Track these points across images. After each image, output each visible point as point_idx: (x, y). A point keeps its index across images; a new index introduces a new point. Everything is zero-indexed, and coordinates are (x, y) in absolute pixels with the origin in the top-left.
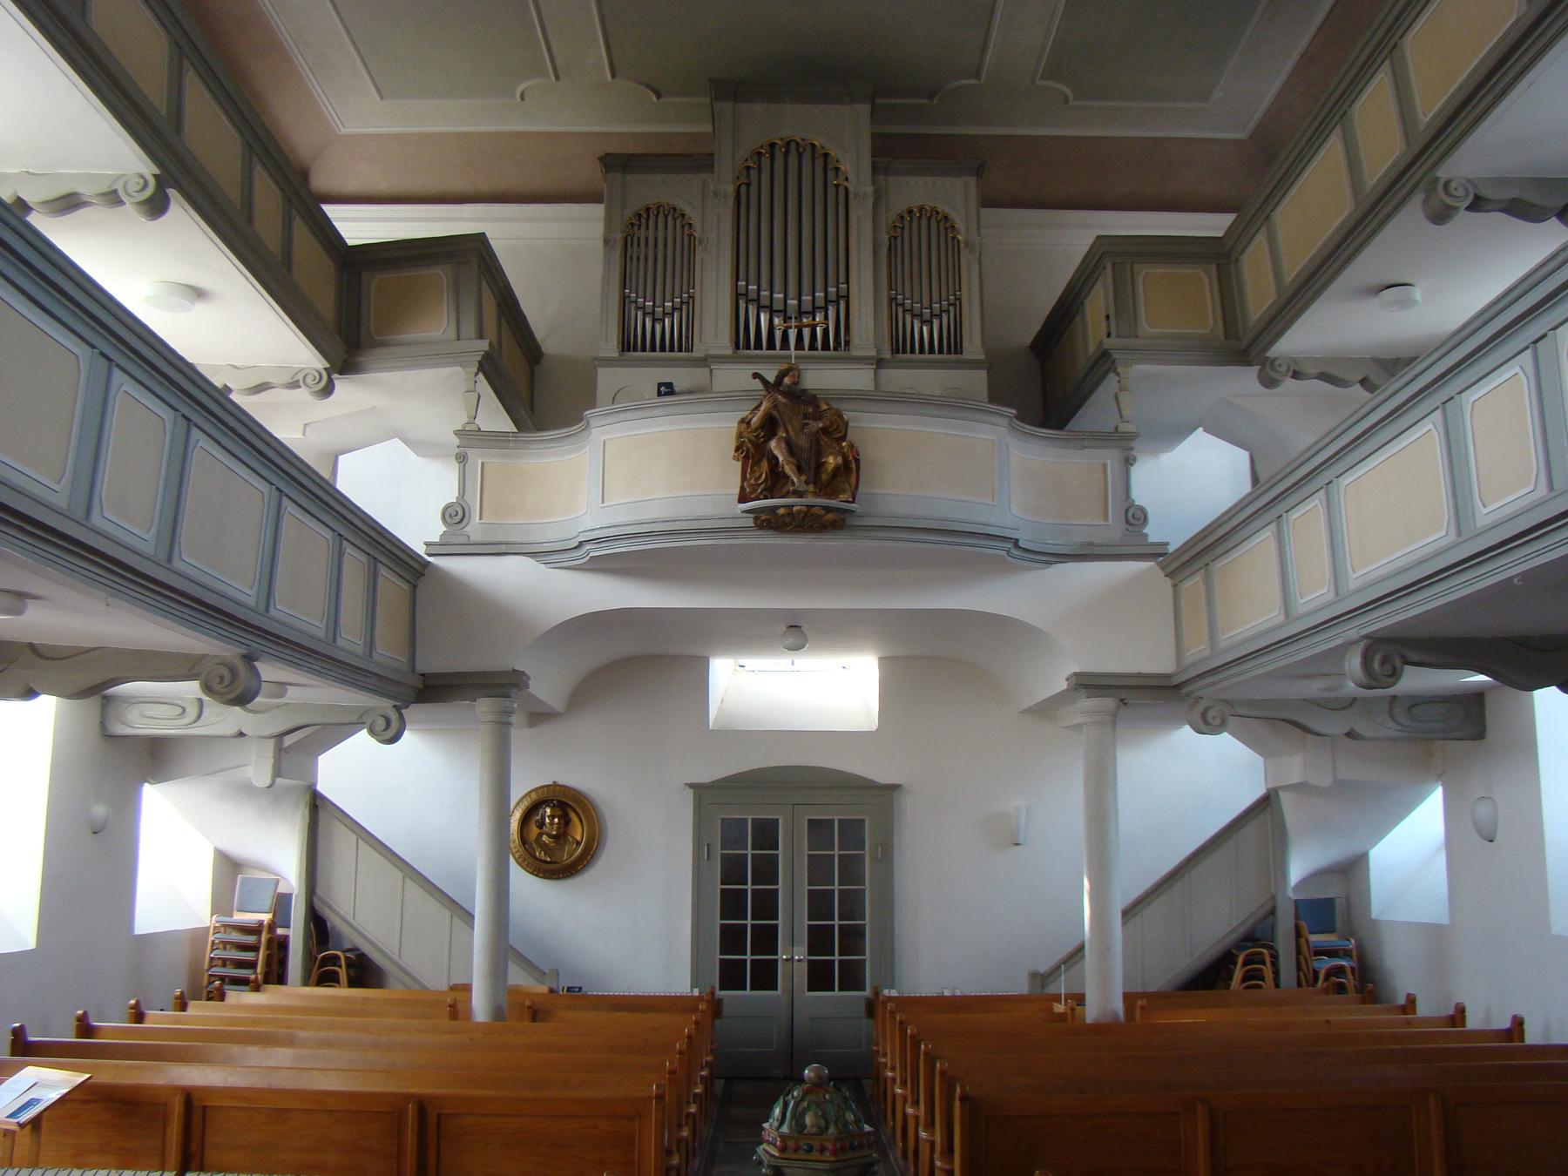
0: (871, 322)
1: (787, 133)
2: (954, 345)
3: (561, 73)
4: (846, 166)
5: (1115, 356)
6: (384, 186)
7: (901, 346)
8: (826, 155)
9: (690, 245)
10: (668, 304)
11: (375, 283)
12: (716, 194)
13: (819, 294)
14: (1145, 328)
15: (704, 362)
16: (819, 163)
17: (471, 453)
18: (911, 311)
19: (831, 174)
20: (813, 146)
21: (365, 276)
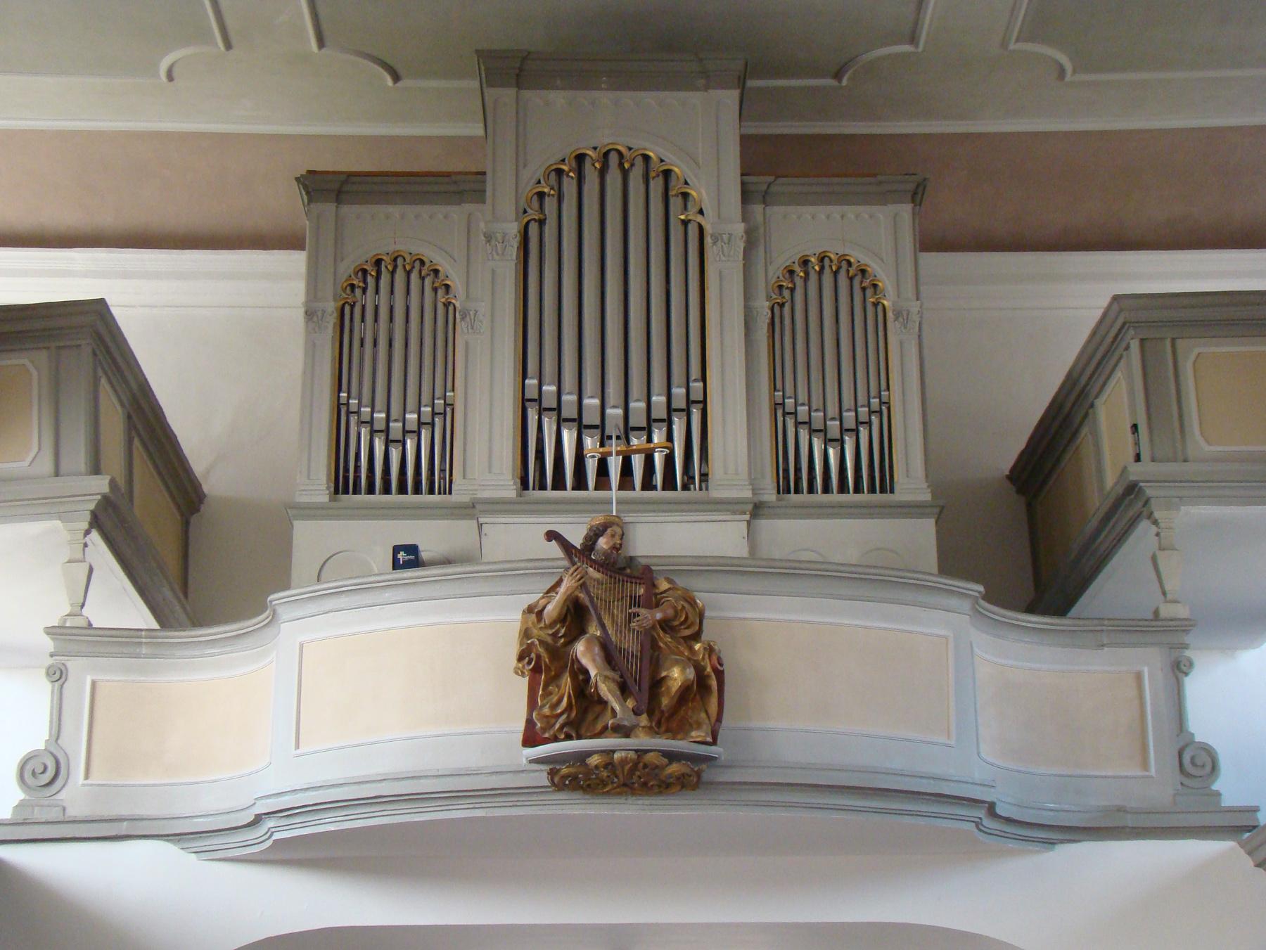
1: (605, 139)
4: (701, 192)
7: (792, 479)
8: (667, 174)
14: (1199, 444)
15: (470, 510)
16: (656, 186)
17: (74, 665)
19: (676, 203)
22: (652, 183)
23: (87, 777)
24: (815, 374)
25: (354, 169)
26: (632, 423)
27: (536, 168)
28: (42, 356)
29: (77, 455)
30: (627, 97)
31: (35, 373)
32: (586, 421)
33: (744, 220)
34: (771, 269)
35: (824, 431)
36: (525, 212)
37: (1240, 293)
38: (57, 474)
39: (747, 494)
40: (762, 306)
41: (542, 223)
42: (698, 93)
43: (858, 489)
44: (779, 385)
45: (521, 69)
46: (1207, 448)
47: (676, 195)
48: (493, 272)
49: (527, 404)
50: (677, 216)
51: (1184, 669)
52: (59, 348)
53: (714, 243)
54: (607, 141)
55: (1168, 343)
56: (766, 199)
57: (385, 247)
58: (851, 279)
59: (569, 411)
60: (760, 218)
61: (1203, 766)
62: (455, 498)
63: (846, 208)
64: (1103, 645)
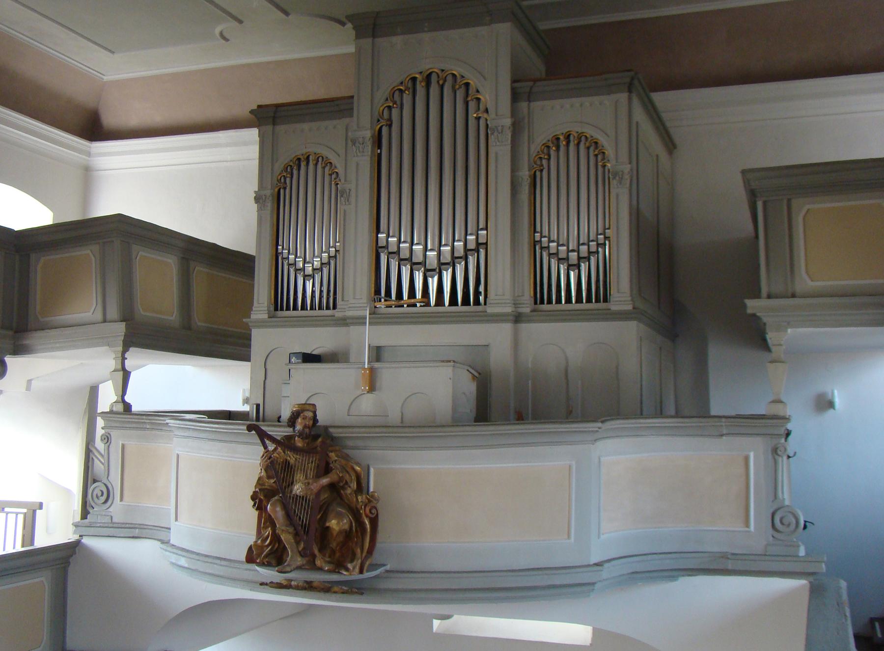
0: (508, 274)
1: (427, 65)
2: (599, 293)
3: (240, 17)
4: (486, 97)
5: (765, 320)
6: (158, 118)
7: (543, 295)
8: (467, 85)
9: (340, 194)
10: (325, 255)
11: (41, 264)
12: (354, 143)
13: (459, 245)
14: (805, 282)
15: (344, 322)
16: (460, 94)
17: (114, 434)
18: (557, 254)
19: (472, 105)
20: (454, 75)
21: (33, 257)
22: (458, 93)
23: (121, 500)
24: (563, 219)
25: (280, 101)
26: (456, 255)
27: (382, 94)
28: (96, 248)
29: (113, 312)
30: (441, 35)
31: (93, 258)
32: (414, 260)
33: (513, 116)
34: (533, 148)
35: (567, 259)
36: (379, 121)
37: (838, 162)
38: (105, 321)
39: (509, 309)
40: (525, 174)
41: (285, 189)
42: (486, 27)
43: (589, 300)
44: (538, 229)
45: (375, 25)
46: (811, 283)
47: (472, 100)
48: (358, 164)
49: (380, 250)
50: (473, 115)
51: (779, 453)
52: (104, 243)
53: (492, 134)
54: (427, 67)
55: (785, 202)
56: (530, 97)
57: (301, 151)
58: (588, 148)
59: (405, 254)
60: (525, 111)
61: (789, 525)
62: (338, 314)
63: (583, 99)
64: (722, 435)
